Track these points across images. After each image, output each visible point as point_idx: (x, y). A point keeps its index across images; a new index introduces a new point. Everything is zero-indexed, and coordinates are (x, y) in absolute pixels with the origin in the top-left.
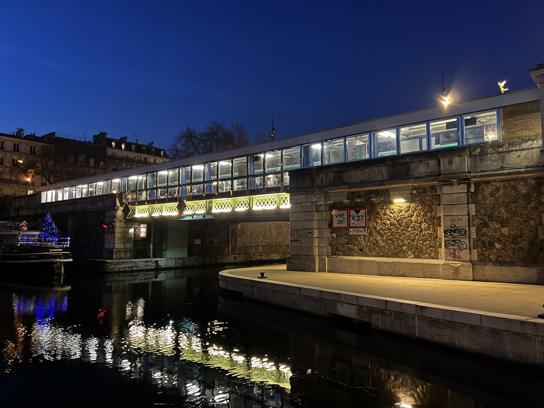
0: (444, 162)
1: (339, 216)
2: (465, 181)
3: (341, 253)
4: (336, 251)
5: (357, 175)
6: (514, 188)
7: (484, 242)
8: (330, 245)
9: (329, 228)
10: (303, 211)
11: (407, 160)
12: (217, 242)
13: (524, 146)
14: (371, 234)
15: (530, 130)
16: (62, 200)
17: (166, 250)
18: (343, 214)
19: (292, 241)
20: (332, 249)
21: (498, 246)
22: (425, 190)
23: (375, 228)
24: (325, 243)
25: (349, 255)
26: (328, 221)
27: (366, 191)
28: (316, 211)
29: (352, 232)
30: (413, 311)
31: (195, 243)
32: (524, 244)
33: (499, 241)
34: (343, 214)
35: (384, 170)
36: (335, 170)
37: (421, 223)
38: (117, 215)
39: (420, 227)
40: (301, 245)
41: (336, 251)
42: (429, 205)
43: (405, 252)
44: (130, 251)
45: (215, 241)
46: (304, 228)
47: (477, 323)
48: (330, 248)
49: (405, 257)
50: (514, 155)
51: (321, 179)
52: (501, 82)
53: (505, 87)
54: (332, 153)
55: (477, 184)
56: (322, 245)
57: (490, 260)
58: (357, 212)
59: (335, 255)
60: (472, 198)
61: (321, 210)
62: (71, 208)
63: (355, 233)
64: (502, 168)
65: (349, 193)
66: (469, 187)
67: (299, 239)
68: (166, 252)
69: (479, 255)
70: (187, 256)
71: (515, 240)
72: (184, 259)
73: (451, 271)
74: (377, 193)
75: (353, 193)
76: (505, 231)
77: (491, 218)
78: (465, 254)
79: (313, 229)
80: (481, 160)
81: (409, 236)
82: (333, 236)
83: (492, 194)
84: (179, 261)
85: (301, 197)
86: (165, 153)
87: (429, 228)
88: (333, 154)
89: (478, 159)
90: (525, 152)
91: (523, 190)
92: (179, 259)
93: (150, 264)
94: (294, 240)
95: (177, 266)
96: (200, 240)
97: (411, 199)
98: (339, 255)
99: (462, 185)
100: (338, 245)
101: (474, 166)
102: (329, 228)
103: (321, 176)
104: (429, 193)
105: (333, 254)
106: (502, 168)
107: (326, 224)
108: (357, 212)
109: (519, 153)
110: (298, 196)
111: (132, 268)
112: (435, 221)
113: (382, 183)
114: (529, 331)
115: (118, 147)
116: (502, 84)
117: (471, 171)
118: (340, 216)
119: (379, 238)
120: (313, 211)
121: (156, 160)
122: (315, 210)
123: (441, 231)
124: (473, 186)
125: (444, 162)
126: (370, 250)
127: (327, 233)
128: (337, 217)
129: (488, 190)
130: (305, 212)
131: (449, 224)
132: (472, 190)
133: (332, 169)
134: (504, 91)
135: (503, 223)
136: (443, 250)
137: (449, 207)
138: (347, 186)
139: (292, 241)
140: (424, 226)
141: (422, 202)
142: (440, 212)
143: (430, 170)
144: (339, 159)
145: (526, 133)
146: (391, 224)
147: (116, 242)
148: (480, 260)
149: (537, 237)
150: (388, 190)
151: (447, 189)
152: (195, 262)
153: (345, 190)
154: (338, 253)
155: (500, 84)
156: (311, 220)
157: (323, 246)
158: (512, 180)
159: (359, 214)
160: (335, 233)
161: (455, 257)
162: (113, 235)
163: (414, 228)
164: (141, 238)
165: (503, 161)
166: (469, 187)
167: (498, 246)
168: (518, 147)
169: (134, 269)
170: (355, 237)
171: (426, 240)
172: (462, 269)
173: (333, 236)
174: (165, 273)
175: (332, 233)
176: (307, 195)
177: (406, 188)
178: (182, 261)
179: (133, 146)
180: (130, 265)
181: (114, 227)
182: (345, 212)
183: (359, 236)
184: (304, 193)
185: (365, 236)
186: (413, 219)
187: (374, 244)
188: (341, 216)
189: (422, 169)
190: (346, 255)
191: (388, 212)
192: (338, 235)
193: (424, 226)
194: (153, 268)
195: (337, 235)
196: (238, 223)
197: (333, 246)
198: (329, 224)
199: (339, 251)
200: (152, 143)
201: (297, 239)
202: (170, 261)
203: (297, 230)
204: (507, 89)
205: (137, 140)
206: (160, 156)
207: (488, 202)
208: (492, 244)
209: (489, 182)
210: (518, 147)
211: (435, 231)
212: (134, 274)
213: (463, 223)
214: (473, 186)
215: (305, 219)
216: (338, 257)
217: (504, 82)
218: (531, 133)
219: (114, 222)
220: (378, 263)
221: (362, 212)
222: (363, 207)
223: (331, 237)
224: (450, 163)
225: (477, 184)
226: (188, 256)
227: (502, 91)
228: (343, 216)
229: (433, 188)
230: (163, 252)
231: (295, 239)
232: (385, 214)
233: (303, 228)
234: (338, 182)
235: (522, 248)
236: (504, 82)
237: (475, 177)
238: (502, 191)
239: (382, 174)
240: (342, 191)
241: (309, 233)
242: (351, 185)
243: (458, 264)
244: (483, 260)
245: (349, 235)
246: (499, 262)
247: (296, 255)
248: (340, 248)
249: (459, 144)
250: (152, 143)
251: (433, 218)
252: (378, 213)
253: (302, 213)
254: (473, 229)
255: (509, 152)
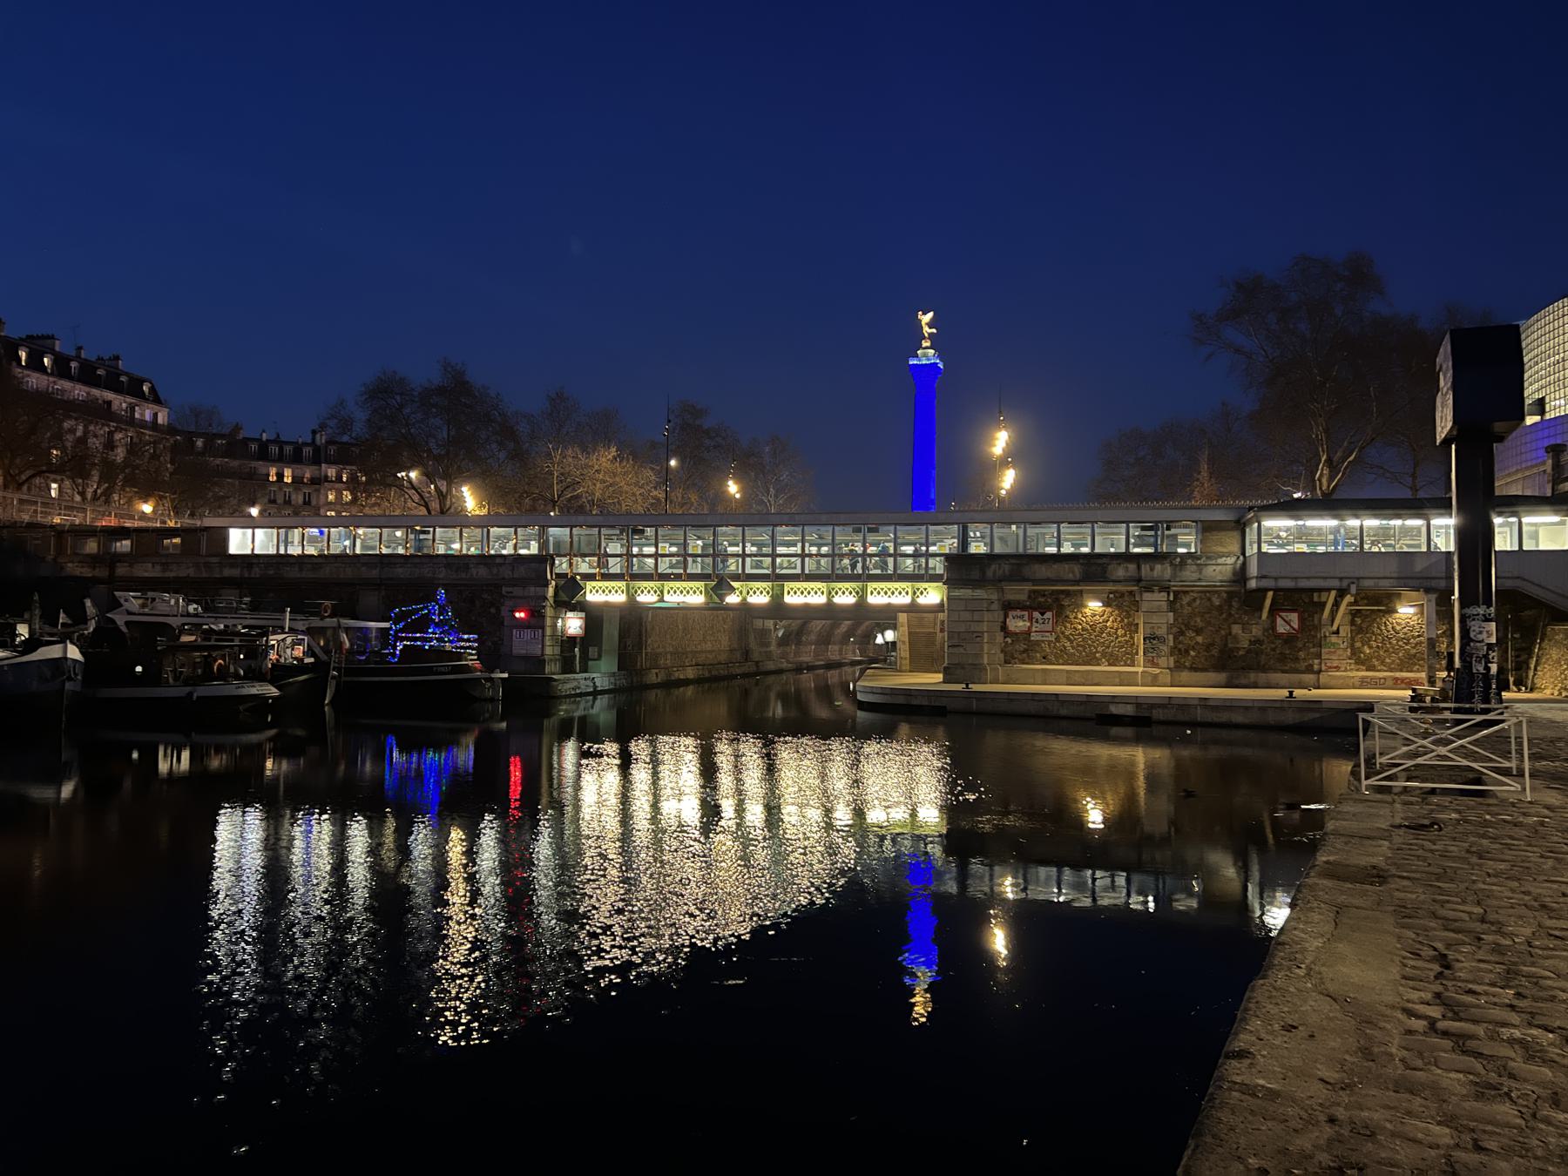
0: (1145, 569)
2: (1166, 589)
5: (1043, 571)
6: (1209, 599)
7: (1180, 650)
8: (1002, 651)
11: (1104, 560)
13: (1220, 561)
14: (1058, 639)
15: (1225, 547)
16: (275, 552)
21: (1192, 653)
22: (1122, 595)
23: (1063, 633)
24: (996, 650)
25: (1027, 663)
27: (1053, 591)
30: (1196, 702)
32: (1215, 652)
33: (1193, 649)
35: (1076, 570)
36: (1013, 561)
37: (1117, 629)
39: (1116, 633)
42: (1127, 611)
43: (1098, 659)
47: (1250, 704)
48: (1002, 656)
49: (1099, 665)
50: (1211, 569)
51: (992, 570)
52: (925, 313)
53: (930, 325)
55: (1176, 594)
57: (1185, 667)
58: (1042, 614)
60: (1172, 606)
62: (375, 573)
63: (1039, 638)
64: (1200, 580)
65: (1030, 591)
66: (1169, 595)
69: (1175, 662)
71: (1208, 647)
73: (1150, 678)
74: (1068, 593)
75: (1034, 591)
76: (1199, 639)
77: (1187, 626)
78: (1163, 661)
79: (983, 633)
80: (1181, 570)
81: (1103, 643)
83: (1189, 604)
86: (152, 389)
87: (1125, 635)
89: (1178, 568)
90: (1220, 567)
91: (1217, 602)
97: (1107, 604)
99: (1163, 594)
101: (1174, 575)
102: (1002, 631)
103: (993, 567)
104: (1126, 598)
105: (1006, 662)
106: (1200, 580)
108: (1042, 614)
109: (1214, 567)
112: (1132, 628)
113: (1077, 582)
114: (1285, 705)
115: (35, 364)
116: (927, 318)
119: (1068, 644)
121: (155, 415)
123: (1139, 638)
124: (1172, 595)
125: (1145, 569)
126: (1056, 657)
127: (999, 637)
129: (1186, 599)
131: (1149, 631)
132: (1171, 598)
135: (1198, 631)
136: (1140, 657)
138: (1031, 583)
140: (1120, 632)
141: (1119, 607)
142: (1139, 618)
143: (1129, 574)
145: (1220, 549)
146: (1083, 629)
148: (1176, 667)
149: (1226, 645)
150: (1081, 591)
151: (1147, 596)
153: (1028, 587)
158: (1209, 592)
159: (1045, 616)
161: (1155, 665)
163: (1109, 634)
165: (1200, 573)
166: (1169, 595)
167: (1192, 653)
168: (1214, 562)
170: (1038, 643)
171: (1122, 647)
172: (1161, 675)
177: (1102, 592)
179: (73, 365)
180: (575, 684)
181: (543, 617)
182: (1026, 613)
183: (1043, 641)
185: (1050, 642)
186: (1108, 624)
187: (1061, 651)
189: (1120, 572)
190: (1024, 663)
191: (1080, 616)
193: (1120, 632)
200: (117, 358)
204: (934, 331)
205: (80, 348)
206: (141, 395)
207: (1185, 611)
208: (1187, 651)
209: (1187, 592)
210: (1214, 562)
211: (1132, 638)
213: (1162, 631)
214: (1172, 595)
217: (931, 315)
218: (1225, 550)
219: (544, 607)
220: (1068, 671)
221: (1049, 615)
222: (1049, 609)
224: (1152, 569)
225: (1176, 594)
229: (1131, 593)
232: (1075, 618)
234: (1016, 577)
235: (1213, 656)
237: (1174, 586)
238: (1198, 602)
239: (1073, 572)
242: (1035, 582)
243: (1157, 671)
244: (1179, 667)
245: (1030, 641)
246: (1193, 669)
249: (1156, 549)
251: (1130, 624)
252: (1067, 617)
254: (1171, 637)
255: (1206, 565)
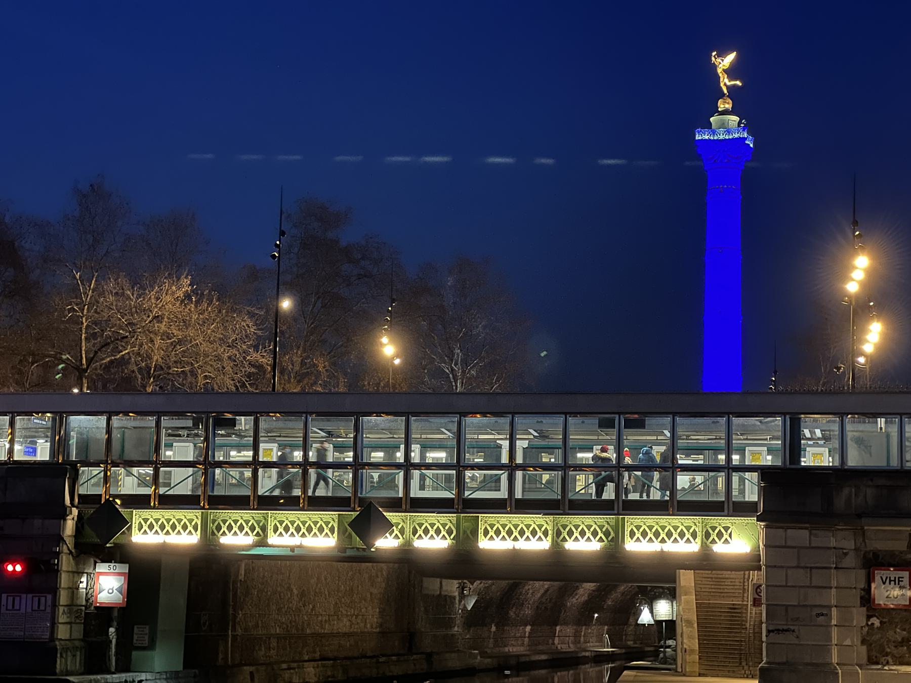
1: (890, 581)
3: (890, 660)
4: (878, 655)
8: (863, 642)
9: (862, 605)
10: (802, 565)
17: (151, 646)
18: (899, 578)
19: (773, 631)
20: (869, 651)
26: (859, 591)
28: (836, 568)
29: (317, 590)
34: (899, 578)
36: (881, 482)
38: (65, 535)
40: (797, 642)
41: (878, 655)
46: (806, 603)
52: (722, 54)
53: (731, 72)
54: (851, 440)
56: (848, 642)
59: (878, 663)
61: (846, 566)
67: (792, 628)
68: (149, 653)
70: (182, 669)
82: (873, 624)
85: (800, 536)
88: (857, 443)
94: (778, 630)
98: (888, 663)
100: (885, 643)
103: (846, 491)
105: (872, 661)
107: (855, 598)
110: (789, 531)
118: (892, 583)
120: (831, 568)
122: (834, 566)
127: (859, 616)
128: (884, 583)
130: (807, 568)
133: (872, 480)
134: (728, 87)
139: (773, 631)
144: (871, 456)
147: (60, 621)
154: (883, 659)
155: (719, 60)
156: (825, 588)
157: (850, 644)
160: (878, 618)
162: (49, 597)
164: (96, 608)
173: (873, 624)
175: (869, 617)
176: (814, 532)
184: (808, 525)
188: (895, 581)
192: (885, 623)
195: (881, 622)
196: (241, 561)
197: (871, 644)
198: (862, 598)
199: (887, 654)
201: (785, 627)
203: (787, 606)
215: (808, 584)
216: (886, 668)
217: (731, 58)
223: (867, 625)
226: (184, 668)
227: (722, 85)
228: (899, 581)
230: (134, 653)
231: (780, 627)
233: (801, 604)
236: (731, 58)
240: (900, 530)
241: (818, 615)
247: (784, 664)
248: (889, 650)
253: (802, 571)
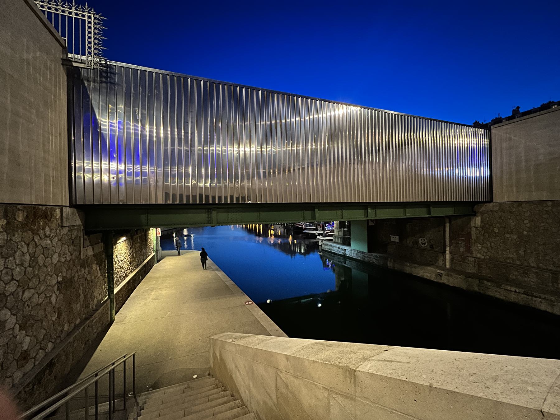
12: (425, 244)
31: (392, 240)
44: (340, 238)
45: (420, 242)
72: (364, 254)
84: (360, 254)
92: (360, 252)
93: (340, 250)
95: (358, 258)
96: (398, 237)
111: (331, 250)
117: (208, 255)
137: (107, 364)
152: (374, 260)
169: (332, 251)
174: (349, 261)
178: (362, 255)
194: (342, 254)
200: (518, 108)
202: (353, 252)
212: (332, 255)
250: (518, 108)
